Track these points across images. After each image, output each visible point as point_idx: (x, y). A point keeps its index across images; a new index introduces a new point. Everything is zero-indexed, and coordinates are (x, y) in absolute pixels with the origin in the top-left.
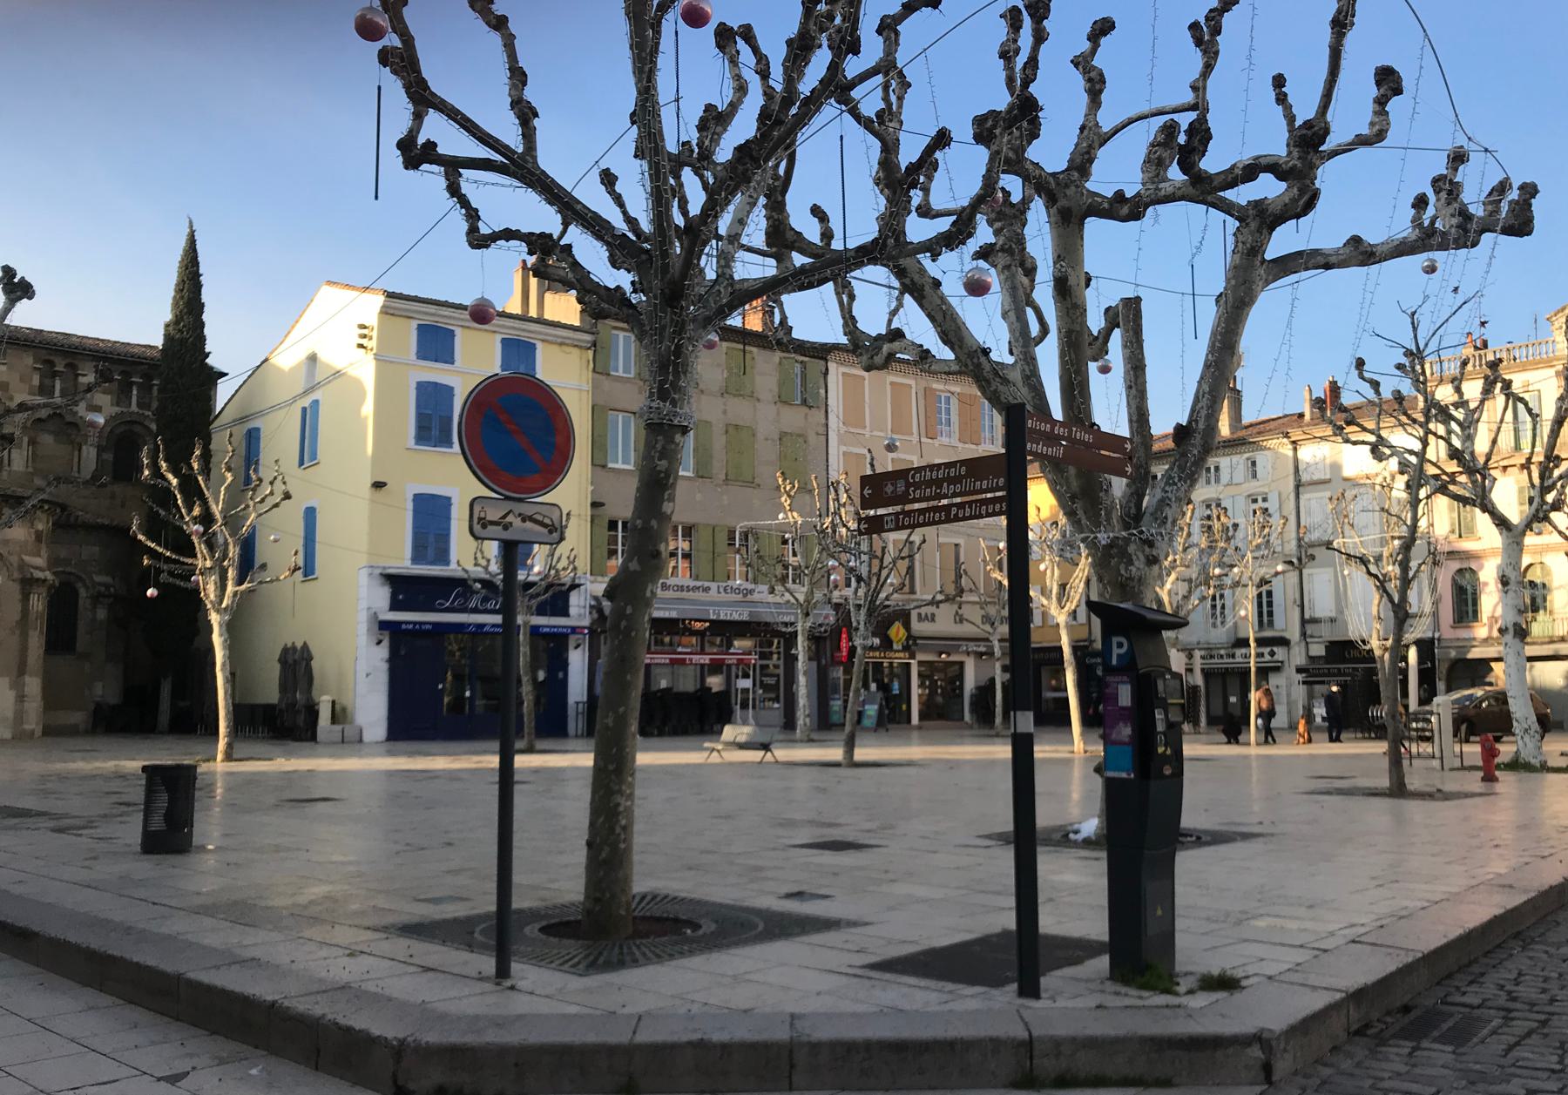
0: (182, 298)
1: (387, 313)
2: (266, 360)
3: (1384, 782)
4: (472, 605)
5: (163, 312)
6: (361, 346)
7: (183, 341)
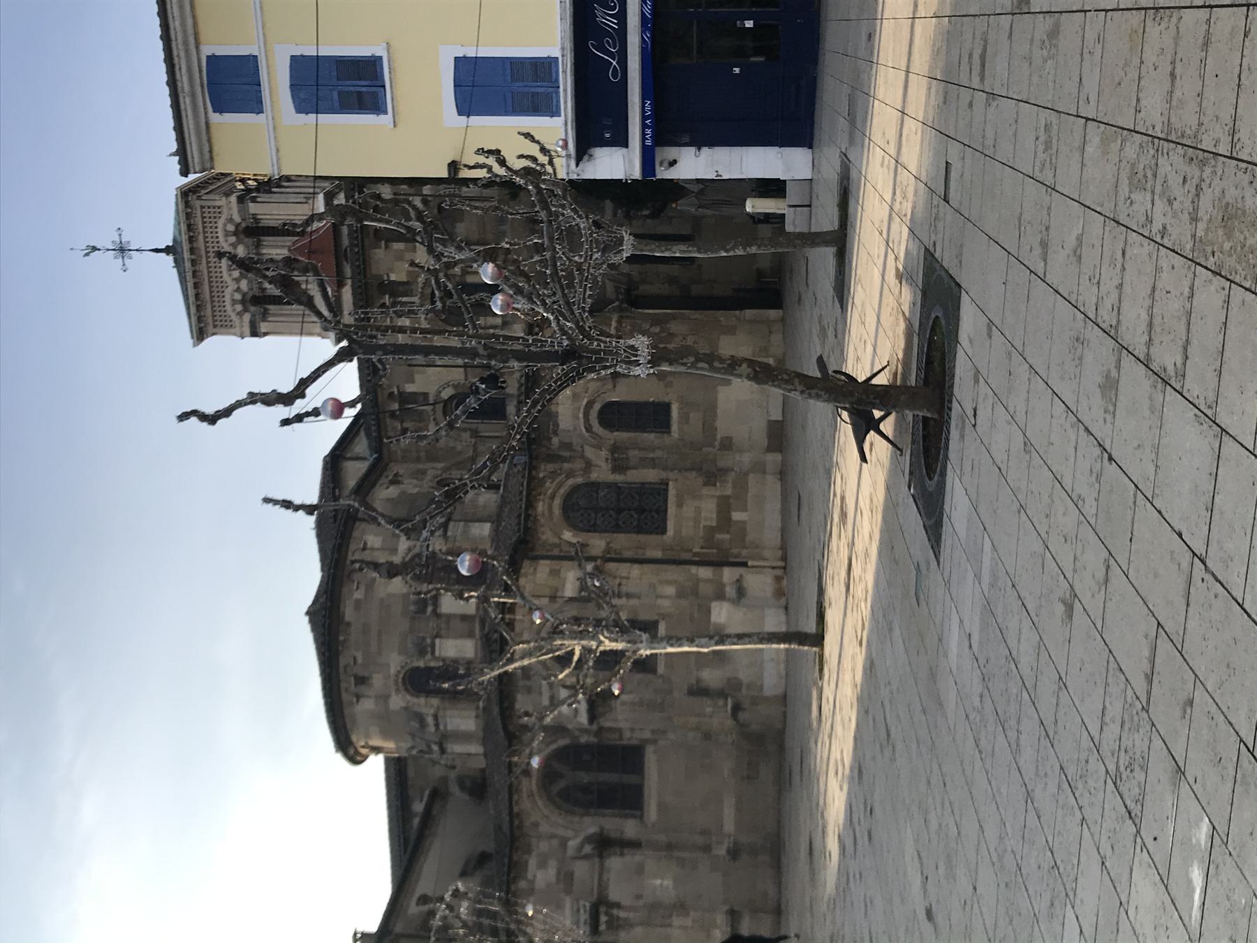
3: (809, 208)
4: (613, 23)
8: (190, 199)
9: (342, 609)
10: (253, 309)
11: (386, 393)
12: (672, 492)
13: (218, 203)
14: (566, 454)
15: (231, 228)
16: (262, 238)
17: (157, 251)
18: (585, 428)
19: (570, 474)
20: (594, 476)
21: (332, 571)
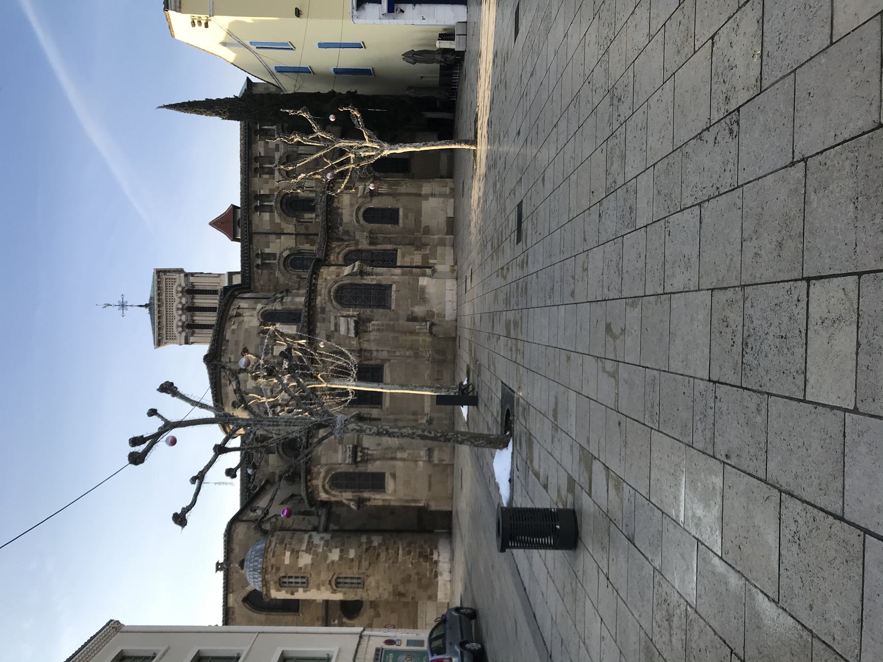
0: (205, 112)
1: (180, 7)
2: (232, 64)
5: (215, 122)
6: (206, 25)
7: (231, 111)
9: (225, 333)
10: (187, 330)
12: (399, 252)
13: (174, 277)
14: (345, 238)
15: (180, 289)
17: (141, 306)
19: (347, 246)
20: (360, 247)
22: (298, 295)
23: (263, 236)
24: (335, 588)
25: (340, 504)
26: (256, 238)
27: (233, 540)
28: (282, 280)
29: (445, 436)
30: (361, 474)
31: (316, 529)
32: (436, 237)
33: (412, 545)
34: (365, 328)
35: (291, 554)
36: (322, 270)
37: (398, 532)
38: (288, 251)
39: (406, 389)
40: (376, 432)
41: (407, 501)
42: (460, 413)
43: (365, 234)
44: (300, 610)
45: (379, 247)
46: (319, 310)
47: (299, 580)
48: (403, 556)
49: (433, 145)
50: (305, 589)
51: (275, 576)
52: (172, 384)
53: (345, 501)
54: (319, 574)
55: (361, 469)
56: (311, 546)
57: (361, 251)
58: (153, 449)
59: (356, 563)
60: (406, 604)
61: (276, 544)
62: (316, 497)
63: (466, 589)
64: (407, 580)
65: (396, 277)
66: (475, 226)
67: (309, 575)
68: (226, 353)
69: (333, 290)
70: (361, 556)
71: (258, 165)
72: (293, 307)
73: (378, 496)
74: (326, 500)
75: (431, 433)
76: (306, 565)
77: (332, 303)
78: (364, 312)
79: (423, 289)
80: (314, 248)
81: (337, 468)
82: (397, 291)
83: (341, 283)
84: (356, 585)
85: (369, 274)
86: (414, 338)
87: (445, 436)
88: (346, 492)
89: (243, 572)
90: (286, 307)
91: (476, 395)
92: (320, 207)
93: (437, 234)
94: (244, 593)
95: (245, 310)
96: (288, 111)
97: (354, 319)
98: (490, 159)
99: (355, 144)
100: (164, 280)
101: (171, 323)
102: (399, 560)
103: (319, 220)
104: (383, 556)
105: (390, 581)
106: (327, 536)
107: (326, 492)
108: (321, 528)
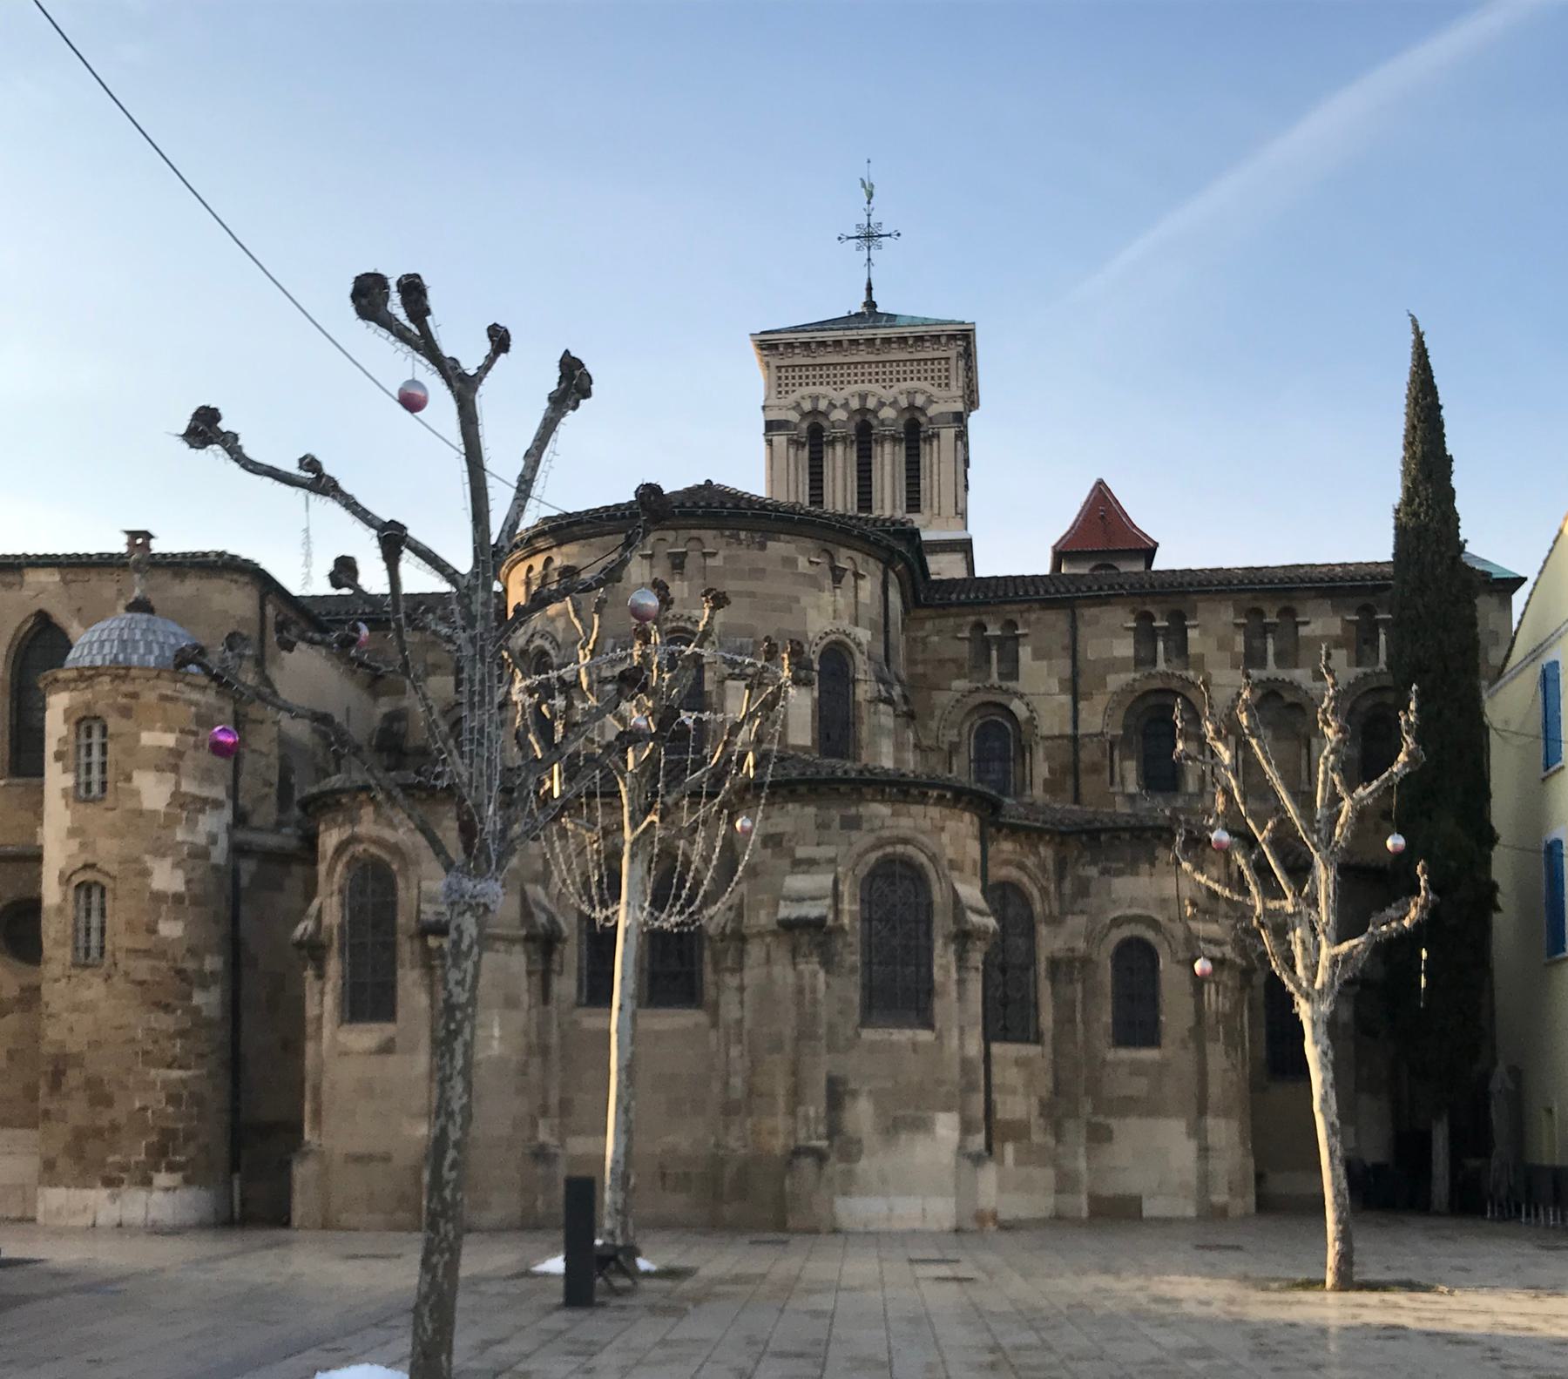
0: (1413, 456)
2: (1561, 531)
5: (1389, 489)
8: (959, 343)
10: (805, 425)
11: (1016, 617)
12: (1031, 1050)
13: (953, 383)
14: (1067, 886)
15: (920, 400)
16: (904, 445)
17: (869, 289)
18: (1120, 917)
19: (1044, 891)
20: (1043, 930)
21: (546, 527)
22: (899, 746)
23: (1067, 641)
24: (76, 880)
25: (310, 892)
26: (1057, 621)
27: (209, 577)
28: (942, 699)
29: (443, 1214)
30: (390, 947)
31: (240, 819)
32: (1082, 1164)
33: (195, 1110)
34: (805, 949)
35: (170, 750)
36: (967, 816)
37: (235, 1064)
38: (1027, 714)
39: (619, 1083)
40: (454, 1000)
41: (317, 1090)
42: (552, 1253)
43: (1081, 945)
44: (17, 781)
45: (1045, 989)
46: (853, 811)
47: (96, 775)
48: (166, 1084)
49: (1332, 1154)
50: (71, 793)
51: (108, 705)
52: (587, 394)
53: (316, 903)
54: (115, 833)
55: (406, 950)
56: (191, 807)
57: (1030, 932)
58: (399, 344)
59: (142, 942)
60: (31, 1092)
61: (197, 704)
62: (330, 816)
63: (57, 1275)
64: (99, 1096)
65: (955, 1042)
66: (1097, 1290)
67: (110, 799)
68: (728, 544)
69: (910, 850)
70: (162, 955)
71: (1271, 618)
72: (864, 732)
73: (329, 1001)
74: (320, 849)
75: (452, 1168)
76: (136, 794)
77: (874, 848)
78: (850, 945)
79: (922, 1125)
80: (1038, 793)
81: (407, 879)
82: (915, 1046)
83: (932, 875)
84: (82, 943)
85: (961, 959)
86: (781, 1103)
87: (443, 1214)
88: (342, 905)
89: (121, 610)
90: (864, 714)
91: (597, 1300)
92: (1161, 808)
93: (1089, 1169)
94: (61, 615)
95: (851, 595)
96: (1412, 706)
97: (831, 917)
98: (1284, 1337)
99: (1324, 913)
100: (945, 355)
101: (923, 374)
102: (153, 1072)
103: (1122, 808)
104: (165, 1022)
105: (95, 1044)
106: (219, 854)
107: (340, 849)
108: (241, 836)
